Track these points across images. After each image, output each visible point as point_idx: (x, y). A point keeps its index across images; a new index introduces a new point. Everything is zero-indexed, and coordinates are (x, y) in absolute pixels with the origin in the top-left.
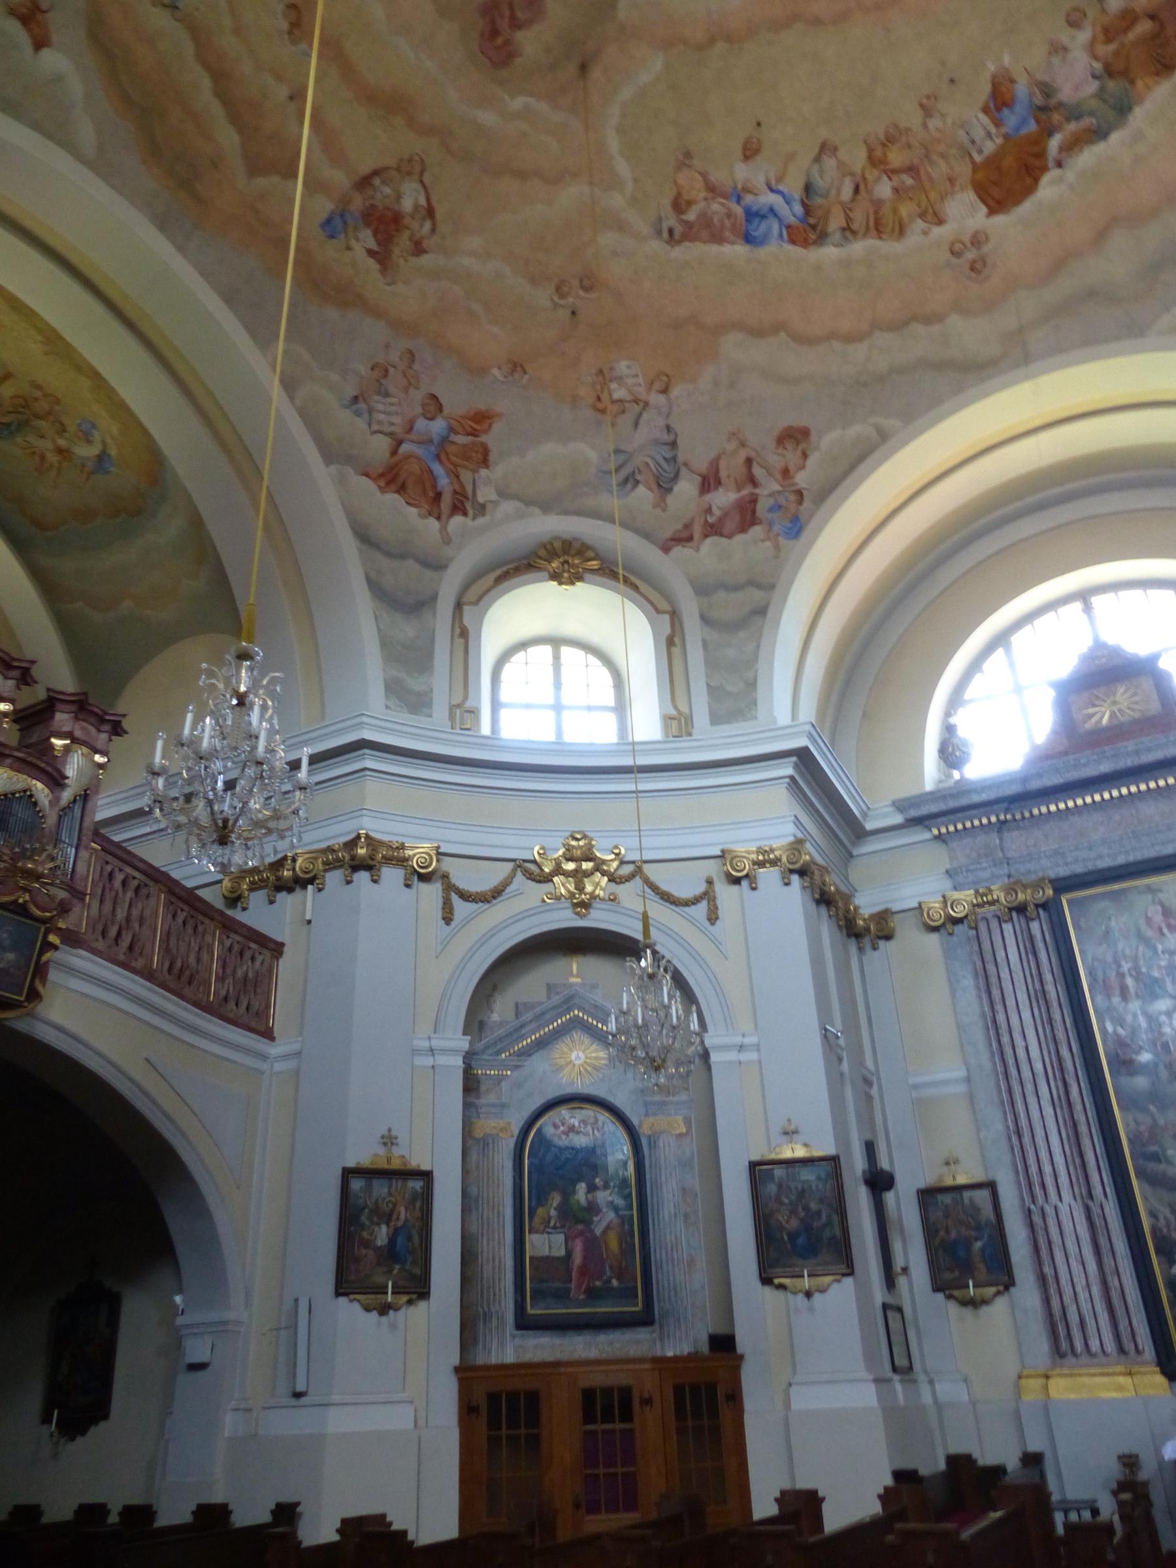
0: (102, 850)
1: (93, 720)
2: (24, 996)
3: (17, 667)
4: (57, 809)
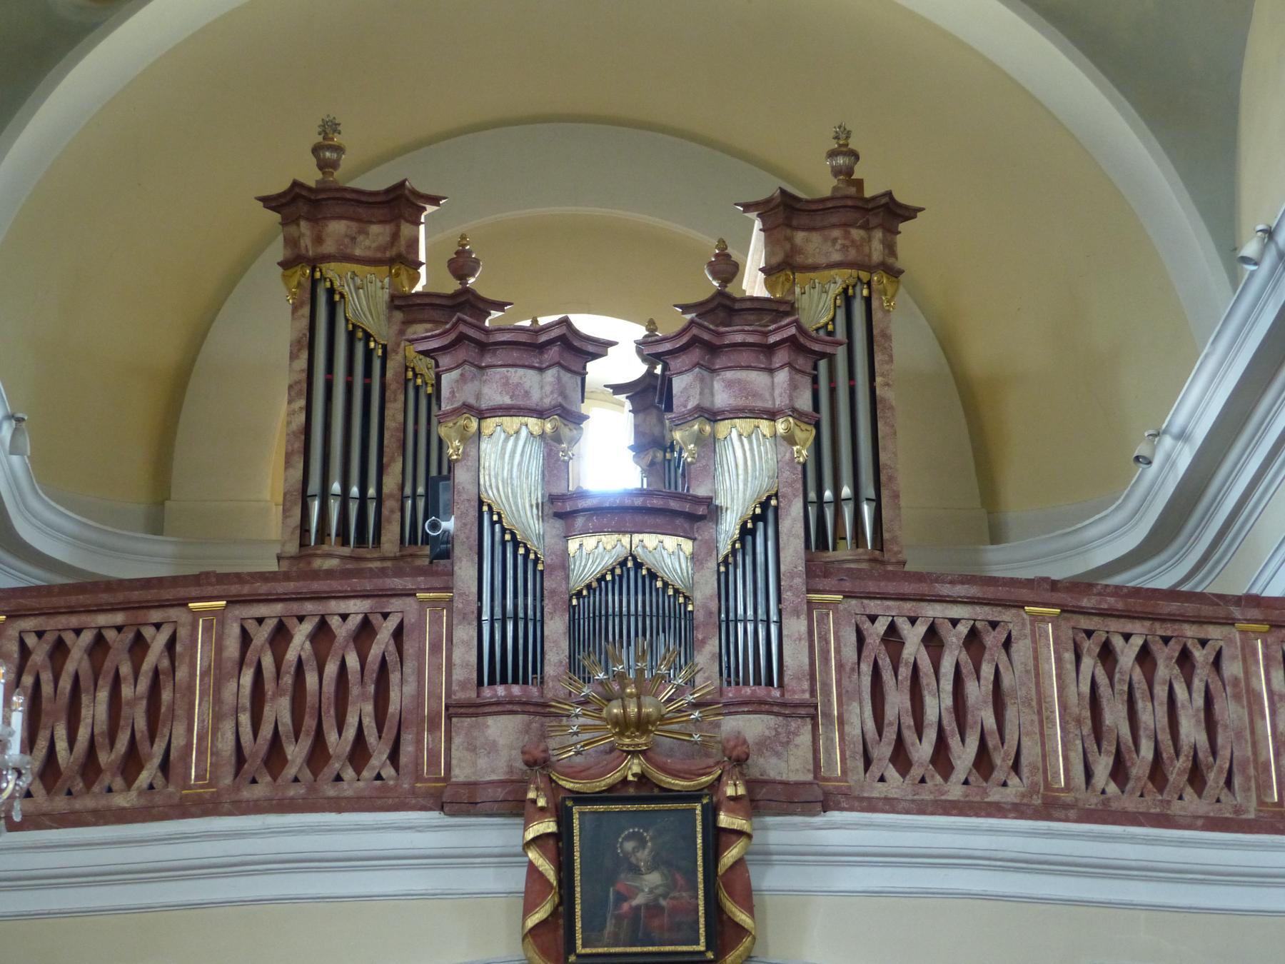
0: (845, 597)
1: (745, 357)
2: (702, 939)
3: (551, 342)
4: (712, 565)
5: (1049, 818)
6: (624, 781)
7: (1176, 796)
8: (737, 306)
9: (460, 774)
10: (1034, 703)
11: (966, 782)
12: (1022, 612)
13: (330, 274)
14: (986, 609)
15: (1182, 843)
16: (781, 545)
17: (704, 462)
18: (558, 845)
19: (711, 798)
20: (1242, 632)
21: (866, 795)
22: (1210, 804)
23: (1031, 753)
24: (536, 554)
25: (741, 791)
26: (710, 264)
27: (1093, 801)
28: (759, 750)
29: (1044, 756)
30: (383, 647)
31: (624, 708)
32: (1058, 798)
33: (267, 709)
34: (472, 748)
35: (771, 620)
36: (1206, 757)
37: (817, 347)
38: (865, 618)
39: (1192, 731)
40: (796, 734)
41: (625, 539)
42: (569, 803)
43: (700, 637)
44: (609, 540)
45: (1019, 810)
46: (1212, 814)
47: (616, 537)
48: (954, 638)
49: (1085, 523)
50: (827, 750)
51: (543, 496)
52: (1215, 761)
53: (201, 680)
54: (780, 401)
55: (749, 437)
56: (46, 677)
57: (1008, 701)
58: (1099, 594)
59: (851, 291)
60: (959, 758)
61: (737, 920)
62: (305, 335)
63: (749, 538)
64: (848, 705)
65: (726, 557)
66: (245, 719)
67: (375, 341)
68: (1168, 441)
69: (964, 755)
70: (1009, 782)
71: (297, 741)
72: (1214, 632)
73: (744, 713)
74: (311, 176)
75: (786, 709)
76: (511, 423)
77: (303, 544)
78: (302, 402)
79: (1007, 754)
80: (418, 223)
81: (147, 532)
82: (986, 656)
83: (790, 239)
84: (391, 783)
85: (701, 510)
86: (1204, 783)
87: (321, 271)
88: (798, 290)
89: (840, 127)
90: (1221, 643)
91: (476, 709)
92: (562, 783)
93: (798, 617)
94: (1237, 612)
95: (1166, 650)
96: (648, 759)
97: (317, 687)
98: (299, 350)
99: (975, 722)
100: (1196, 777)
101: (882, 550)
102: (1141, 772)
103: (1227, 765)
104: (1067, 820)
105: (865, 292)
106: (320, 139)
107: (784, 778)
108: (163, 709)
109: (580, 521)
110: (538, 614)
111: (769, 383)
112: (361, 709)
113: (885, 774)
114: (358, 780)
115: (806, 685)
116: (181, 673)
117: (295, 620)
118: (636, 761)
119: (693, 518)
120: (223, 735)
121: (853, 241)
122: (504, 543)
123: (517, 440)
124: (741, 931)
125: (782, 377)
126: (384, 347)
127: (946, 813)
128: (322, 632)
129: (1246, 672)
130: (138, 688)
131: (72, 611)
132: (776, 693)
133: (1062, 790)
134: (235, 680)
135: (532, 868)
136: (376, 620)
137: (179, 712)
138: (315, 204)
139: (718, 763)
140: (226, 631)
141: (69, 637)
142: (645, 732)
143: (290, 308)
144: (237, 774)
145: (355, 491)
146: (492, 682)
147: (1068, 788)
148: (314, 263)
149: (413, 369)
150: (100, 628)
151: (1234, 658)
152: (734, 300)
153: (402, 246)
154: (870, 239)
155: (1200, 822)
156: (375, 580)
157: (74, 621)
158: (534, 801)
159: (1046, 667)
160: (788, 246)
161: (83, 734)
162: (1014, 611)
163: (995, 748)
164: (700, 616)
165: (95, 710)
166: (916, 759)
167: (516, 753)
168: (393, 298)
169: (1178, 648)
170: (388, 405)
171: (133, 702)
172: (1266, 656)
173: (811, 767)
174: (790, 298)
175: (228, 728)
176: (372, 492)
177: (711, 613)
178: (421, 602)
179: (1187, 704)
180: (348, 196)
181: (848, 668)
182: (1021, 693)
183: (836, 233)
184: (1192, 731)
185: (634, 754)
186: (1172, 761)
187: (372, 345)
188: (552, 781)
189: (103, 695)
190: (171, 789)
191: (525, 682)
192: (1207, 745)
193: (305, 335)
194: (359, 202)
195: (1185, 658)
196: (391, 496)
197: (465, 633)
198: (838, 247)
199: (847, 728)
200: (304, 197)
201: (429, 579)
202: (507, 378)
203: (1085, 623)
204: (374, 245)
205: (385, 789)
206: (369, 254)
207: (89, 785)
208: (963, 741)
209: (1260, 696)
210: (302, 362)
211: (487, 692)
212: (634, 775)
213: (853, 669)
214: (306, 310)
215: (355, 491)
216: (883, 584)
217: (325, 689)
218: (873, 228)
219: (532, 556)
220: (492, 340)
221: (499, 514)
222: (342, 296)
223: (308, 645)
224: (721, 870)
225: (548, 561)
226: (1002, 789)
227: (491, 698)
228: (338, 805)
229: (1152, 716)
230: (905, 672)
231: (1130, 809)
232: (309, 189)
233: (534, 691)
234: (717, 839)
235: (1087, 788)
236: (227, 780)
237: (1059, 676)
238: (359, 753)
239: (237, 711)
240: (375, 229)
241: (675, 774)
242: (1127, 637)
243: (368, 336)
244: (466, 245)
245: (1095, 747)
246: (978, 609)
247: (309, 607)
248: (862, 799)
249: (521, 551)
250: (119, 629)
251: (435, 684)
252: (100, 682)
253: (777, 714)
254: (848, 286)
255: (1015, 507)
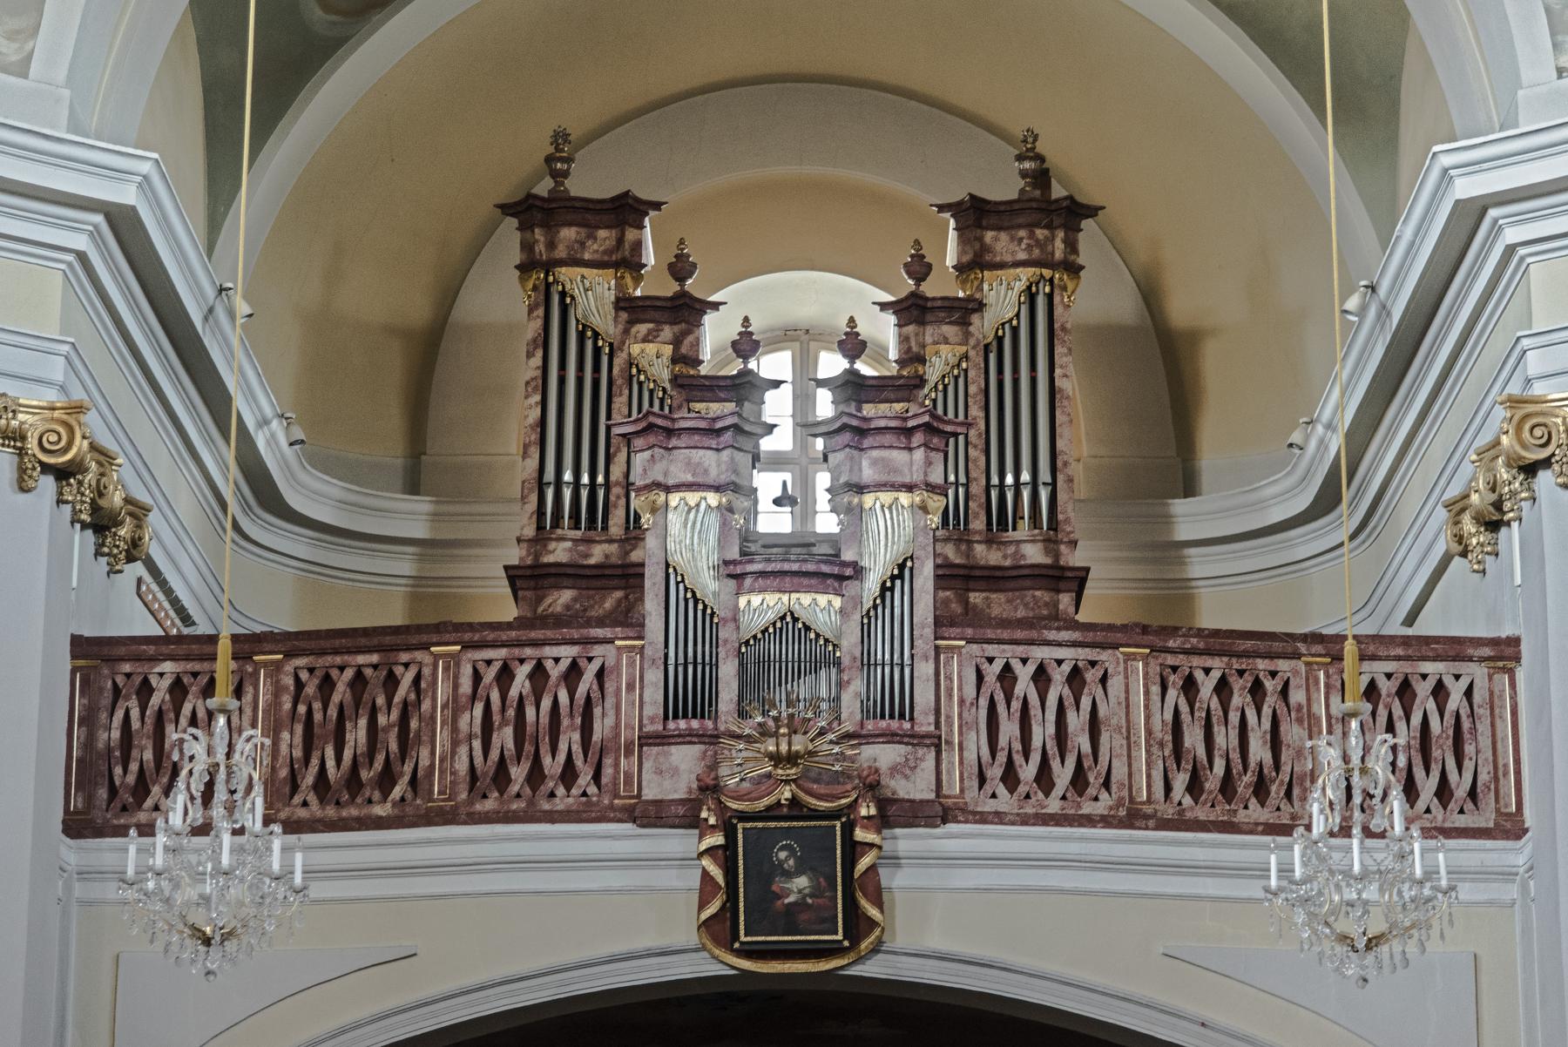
1: (888, 439)
5: (1132, 827)
6: (778, 803)
7: (1242, 806)
8: (929, 304)
9: (649, 794)
10: (1124, 730)
11: (1064, 798)
12: (1117, 652)
13: (562, 278)
14: (1087, 650)
15: (1243, 846)
16: (915, 601)
17: (852, 529)
18: (726, 855)
19: (849, 817)
20: (1308, 664)
21: (979, 809)
22: (1271, 812)
23: (1119, 772)
24: (712, 608)
25: (873, 811)
26: (906, 265)
27: (1169, 812)
28: (891, 773)
29: (1130, 775)
30: (588, 686)
31: (777, 745)
32: (1141, 810)
33: (495, 736)
34: (659, 772)
35: (1040, 482)
36: (1270, 772)
37: (949, 428)
38: (984, 660)
39: (1259, 751)
40: (922, 760)
41: (785, 598)
42: (735, 821)
43: (846, 678)
44: (771, 599)
45: (1106, 821)
46: (1271, 821)
47: (778, 595)
48: (1059, 675)
49: (1262, 483)
50: (949, 772)
51: (718, 560)
52: (1278, 774)
53: (442, 712)
54: (917, 477)
55: (890, 508)
56: (317, 706)
57: (1103, 728)
58: (1184, 636)
59: (1034, 289)
60: (1059, 776)
61: (869, 914)
62: (539, 334)
63: (888, 594)
64: (968, 735)
65: (869, 611)
66: (477, 744)
67: (602, 339)
68: (1320, 429)
69: (1063, 775)
70: (1100, 797)
71: (519, 763)
72: (1283, 665)
73: (879, 743)
74: (544, 188)
75: (914, 739)
76: (692, 498)
77: (540, 527)
78: (538, 398)
79: (1099, 774)
80: (641, 227)
81: (404, 493)
82: (1086, 691)
83: (980, 239)
84: (595, 799)
85: (849, 572)
86: (1268, 793)
87: (553, 274)
88: (986, 287)
89: (1028, 131)
90: (1289, 674)
91: (662, 739)
92: (728, 804)
93: (927, 661)
94: (1303, 648)
95: (1241, 681)
96: (798, 786)
97: (535, 719)
98: (535, 349)
99: (1074, 747)
100: (1261, 790)
101: (1056, 530)
102: (1213, 786)
103: (1287, 779)
104: (1147, 828)
105: (1047, 289)
106: (551, 149)
107: (912, 797)
108: (412, 735)
109: (748, 581)
110: (714, 659)
111: (908, 460)
112: (570, 738)
113: (997, 792)
114: (568, 796)
115: (932, 719)
116: (426, 706)
117: (517, 663)
118: (788, 788)
119: (841, 578)
120: (459, 758)
121: (1037, 241)
122: (686, 600)
123: (697, 511)
124: (873, 924)
125: (919, 455)
126: (611, 345)
127: (1045, 823)
128: (539, 674)
129: (1309, 700)
130: (391, 717)
131: (336, 652)
132: (907, 725)
133: (1143, 803)
134: (469, 712)
135: (705, 874)
136: (582, 663)
137: (424, 738)
138: (549, 212)
139: (854, 788)
140: (461, 671)
141: (334, 673)
142: (796, 765)
143: (526, 310)
144: (471, 791)
145: (585, 479)
146: (676, 717)
147: (1149, 801)
148: (549, 266)
149: (637, 366)
150: (359, 666)
151: (1299, 687)
152: (927, 299)
153: (627, 250)
154: (1053, 238)
155: (1260, 828)
156: (582, 630)
157: (338, 660)
158: (706, 820)
159: (1136, 699)
160: (977, 246)
161: (348, 755)
162: (1110, 651)
163: (1090, 768)
164: (846, 661)
165: (357, 735)
166: (1022, 778)
167: (693, 777)
168: (618, 300)
169: (1251, 679)
170: (615, 399)
171: (387, 729)
172: (1327, 686)
173: (934, 788)
174: (978, 296)
175: (463, 751)
176: (600, 479)
177: (855, 658)
178: (619, 648)
179: (1256, 727)
180: (577, 205)
181: (968, 704)
182: (1114, 721)
183: (1022, 233)
184: (1259, 751)
185: (787, 782)
186: (1240, 776)
187: (600, 343)
188: (721, 802)
189: (363, 722)
190: (418, 801)
191: (703, 717)
192: (1271, 762)
193: (539, 334)
194: (587, 210)
195: (1257, 690)
196: (617, 483)
197: (654, 676)
198: (1023, 246)
199: (966, 754)
200: (537, 206)
201: (626, 629)
202: (690, 459)
203: (1171, 660)
204: (602, 249)
205: (589, 804)
206: (597, 257)
207: (353, 798)
208: (1063, 762)
209: (1319, 720)
210: (537, 360)
211: (671, 725)
212: (786, 800)
213: (972, 704)
214: (540, 312)
215: (585, 479)
216: (999, 631)
217: (541, 721)
218: (1056, 228)
219: (709, 611)
220: (676, 427)
221: (682, 575)
222: (573, 298)
223: (527, 683)
224: (856, 875)
225: (722, 614)
226: (1093, 803)
227: (674, 730)
228: (552, 817)
229: (1225, 738)
230: (1016, 705)
231: (1201, 818)
232: (542, 199)
233: (709, 724)
234: (853, 850)
235: (1165, 801)
236: (464, 796)
237: (1147, 707)
238: (569, 775)
239: (470, 737)
240: (602, 233)
241: (819, 797)
242: (1207, 671)
243: (596, 335)
244: (684, 249)
245: (1175, 765)
246: (1080, 650)
247: (528, 651)
248: (974, 813)
249: (700, 607)
250: (375, 667)
251: (629, 716)
252: (360, 711)
253: (907, 744)
254: (1031, 284)
255: (1210, 459)
